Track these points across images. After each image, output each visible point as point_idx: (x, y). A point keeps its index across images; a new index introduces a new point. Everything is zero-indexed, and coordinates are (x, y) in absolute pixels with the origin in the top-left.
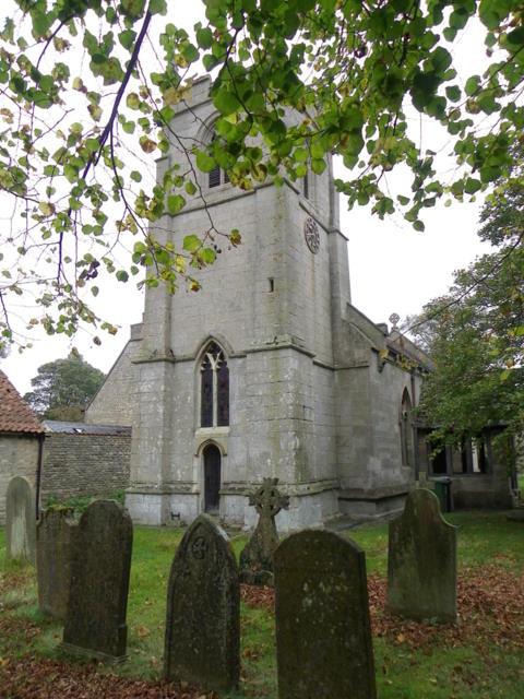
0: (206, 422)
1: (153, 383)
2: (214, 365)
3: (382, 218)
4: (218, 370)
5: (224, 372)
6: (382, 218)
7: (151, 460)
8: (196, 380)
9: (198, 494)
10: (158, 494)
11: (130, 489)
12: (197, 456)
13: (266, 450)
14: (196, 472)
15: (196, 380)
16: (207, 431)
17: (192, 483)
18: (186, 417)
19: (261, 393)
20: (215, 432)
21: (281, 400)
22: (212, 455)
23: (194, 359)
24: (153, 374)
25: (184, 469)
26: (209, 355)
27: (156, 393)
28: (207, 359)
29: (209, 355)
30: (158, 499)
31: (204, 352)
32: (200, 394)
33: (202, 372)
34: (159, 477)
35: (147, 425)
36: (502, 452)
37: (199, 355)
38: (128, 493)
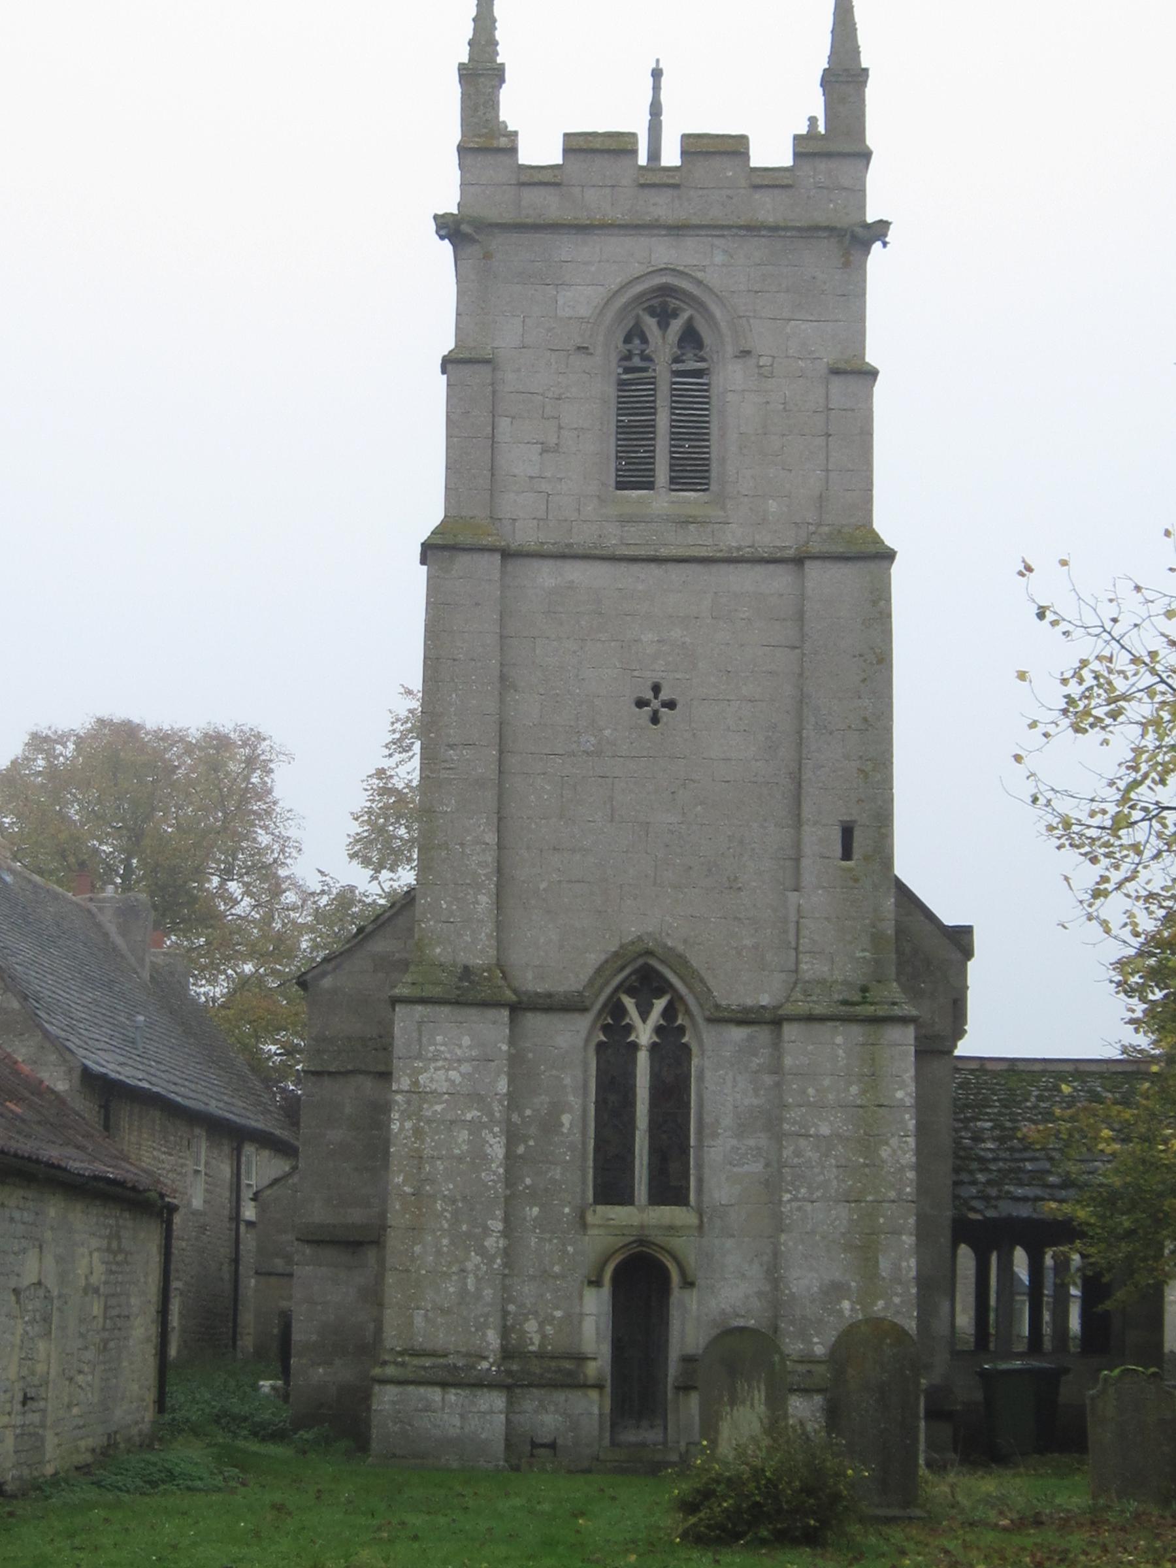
0: (624, 1197)
1: (466, 1068)
2: (644, 1034)
3: (880, 230)
4: (654, 1048)
5: (672, 1051)
6: (880, 230)
7: (463, 1292)
8: (585, 1064)
9: (599, 1387)
10: (491, 1386)
11: (390, 1371)
12: (596, 1283)
13: (837, 1275)
14: (592, 1319)
15: (585, 1064)
16: (619, 1214)
17: (581, 1359)
18: (557, 1173)
19: (825, 1130)
20: (639, 1215)
21: (885, 1152)
22: (642, 1282)
23: (585, 1010)
24: (466, 1041)
25: (550, 1319)
26: (629, 1003)
27: (477, 1098)
28: (618, 1011)
29: (629, 1003)
30: (497, 1401)
31: (617, 990)
32: (592, 1107)
33: (600, 1046)
34: (493, 1338)
35: (448, 1188)
36: (1150, 691)
37: (602, 998)
38: (384, 1381)
